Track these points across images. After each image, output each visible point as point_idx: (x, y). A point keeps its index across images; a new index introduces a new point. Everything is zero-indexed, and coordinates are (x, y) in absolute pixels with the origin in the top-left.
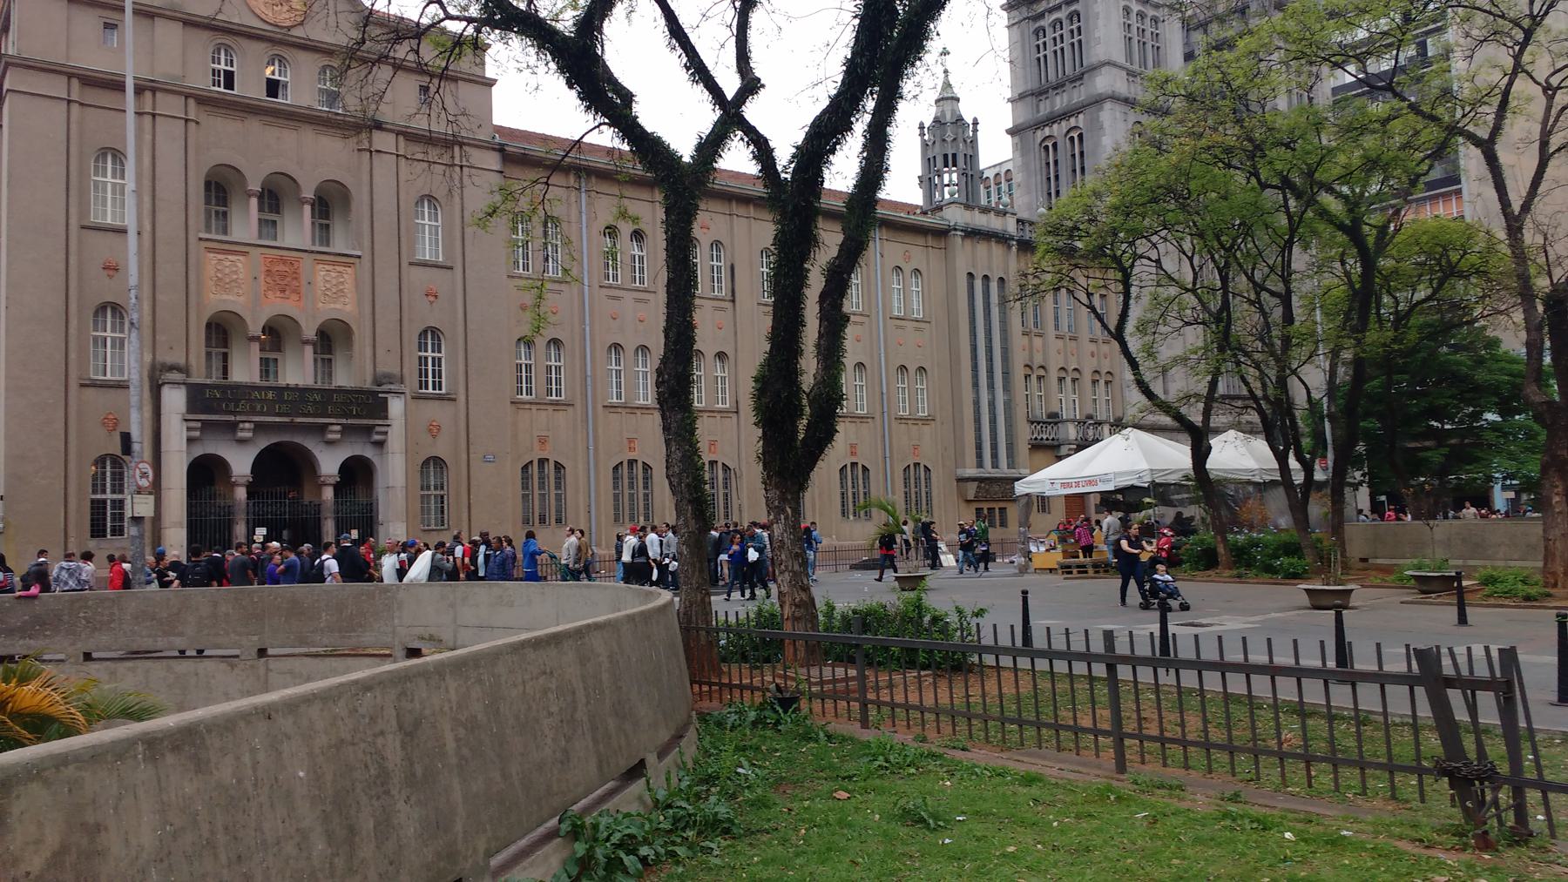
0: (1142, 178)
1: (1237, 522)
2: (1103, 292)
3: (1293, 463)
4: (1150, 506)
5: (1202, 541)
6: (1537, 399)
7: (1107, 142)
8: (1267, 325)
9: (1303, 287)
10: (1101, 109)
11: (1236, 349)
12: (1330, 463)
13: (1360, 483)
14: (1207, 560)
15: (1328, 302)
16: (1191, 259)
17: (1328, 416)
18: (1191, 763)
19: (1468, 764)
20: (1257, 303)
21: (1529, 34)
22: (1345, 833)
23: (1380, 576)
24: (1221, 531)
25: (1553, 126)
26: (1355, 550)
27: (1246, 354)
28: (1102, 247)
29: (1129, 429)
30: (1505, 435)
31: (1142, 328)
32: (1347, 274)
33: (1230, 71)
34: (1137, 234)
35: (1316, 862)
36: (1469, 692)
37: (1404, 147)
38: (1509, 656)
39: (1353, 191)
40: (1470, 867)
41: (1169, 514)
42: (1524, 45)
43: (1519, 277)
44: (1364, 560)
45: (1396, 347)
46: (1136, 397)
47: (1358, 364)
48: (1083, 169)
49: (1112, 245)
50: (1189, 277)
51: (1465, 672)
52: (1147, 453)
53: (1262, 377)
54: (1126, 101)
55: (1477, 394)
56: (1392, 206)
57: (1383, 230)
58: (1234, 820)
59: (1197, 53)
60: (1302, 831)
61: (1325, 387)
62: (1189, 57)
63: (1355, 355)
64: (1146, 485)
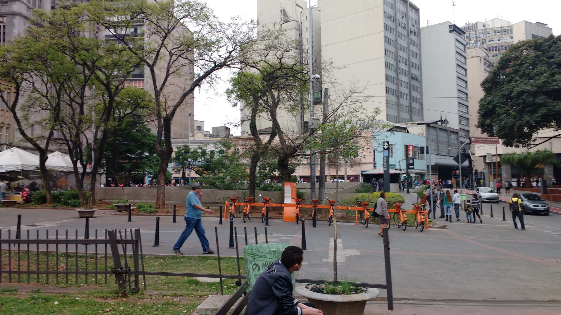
0: (28, 49)
1: (56, 186)
2: (9, 91)
3: (79, 165)
4: (20, 179)
5: (41, 193)
6: (159, 149)
7: (16, 31)
8: (74, 114)
9: (89, 103)
10: (14, 18)
11: (62, 121)
12: (93, 166)
13: (103, 174)
14: (42, 201)
15: (97, 109)
16: (46, 85)
17: (93, 149)
18: (21, 280)
19: (122, 269)
20: (71, 105)
21: (167, 35)
22: (77, 298)
23: (106, 206)
24: (49, 189)
25: (171, 65)
26: (98, 197)
27: (65, 124)
28: (9, 73)
29: (14, 148)
30: (150, 160)
31: (23, 108)
32: (104, 100)
33: (67, 17)
34: (24, 70)
35: (65, 311)
36: (124, 244)
37: (126, 61)
38: (138, 231)
39: (108, 72)
40: (119, 303)
41: (27, 182)
42: (165, 37)
43: (157, 110)
44: (101, 200)
45: (118, 128)
46: (19, 136)
47: (105, 132)
48: (4, 40)
49: (13, 73)
50: (45, 92)
51: (124, 238)
52: (21, 158)
53: (71, 133)
54: (26, 18)
55: (143, 146)
56: (121, 80)
57: (117, 87)
58: (36, 300)
59: (56, 7)
60: (61, 300)
61: (93, 139)
62: (53, 8)
63: (104, 129)
64: (20, 171)
